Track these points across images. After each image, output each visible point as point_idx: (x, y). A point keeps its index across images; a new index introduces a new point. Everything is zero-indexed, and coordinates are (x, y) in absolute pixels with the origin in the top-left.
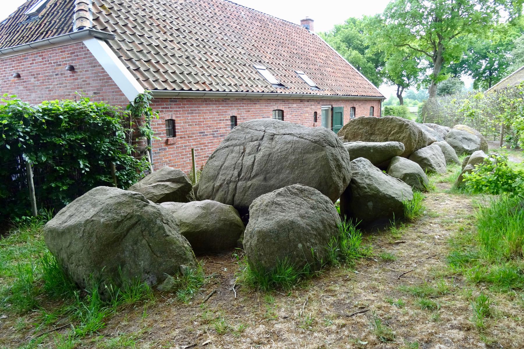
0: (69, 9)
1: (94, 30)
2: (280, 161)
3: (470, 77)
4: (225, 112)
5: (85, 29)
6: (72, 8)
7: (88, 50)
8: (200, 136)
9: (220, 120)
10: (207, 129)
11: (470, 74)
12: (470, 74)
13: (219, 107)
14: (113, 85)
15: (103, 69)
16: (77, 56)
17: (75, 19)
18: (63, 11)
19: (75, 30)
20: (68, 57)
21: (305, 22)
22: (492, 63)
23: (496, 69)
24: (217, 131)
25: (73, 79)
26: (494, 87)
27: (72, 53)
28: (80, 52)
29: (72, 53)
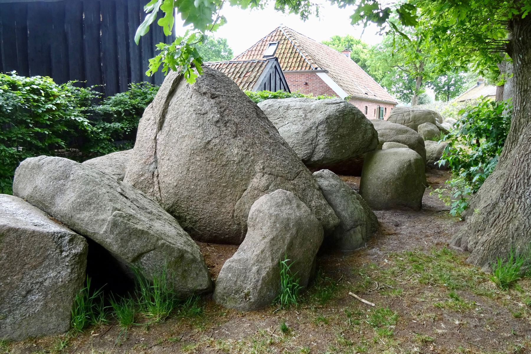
2: (419, 117)
3: (433, 90)
11: (433, 88)
12: (433, 88)
22: (450, 80)
23: (452, 85)
26: (452, 100)
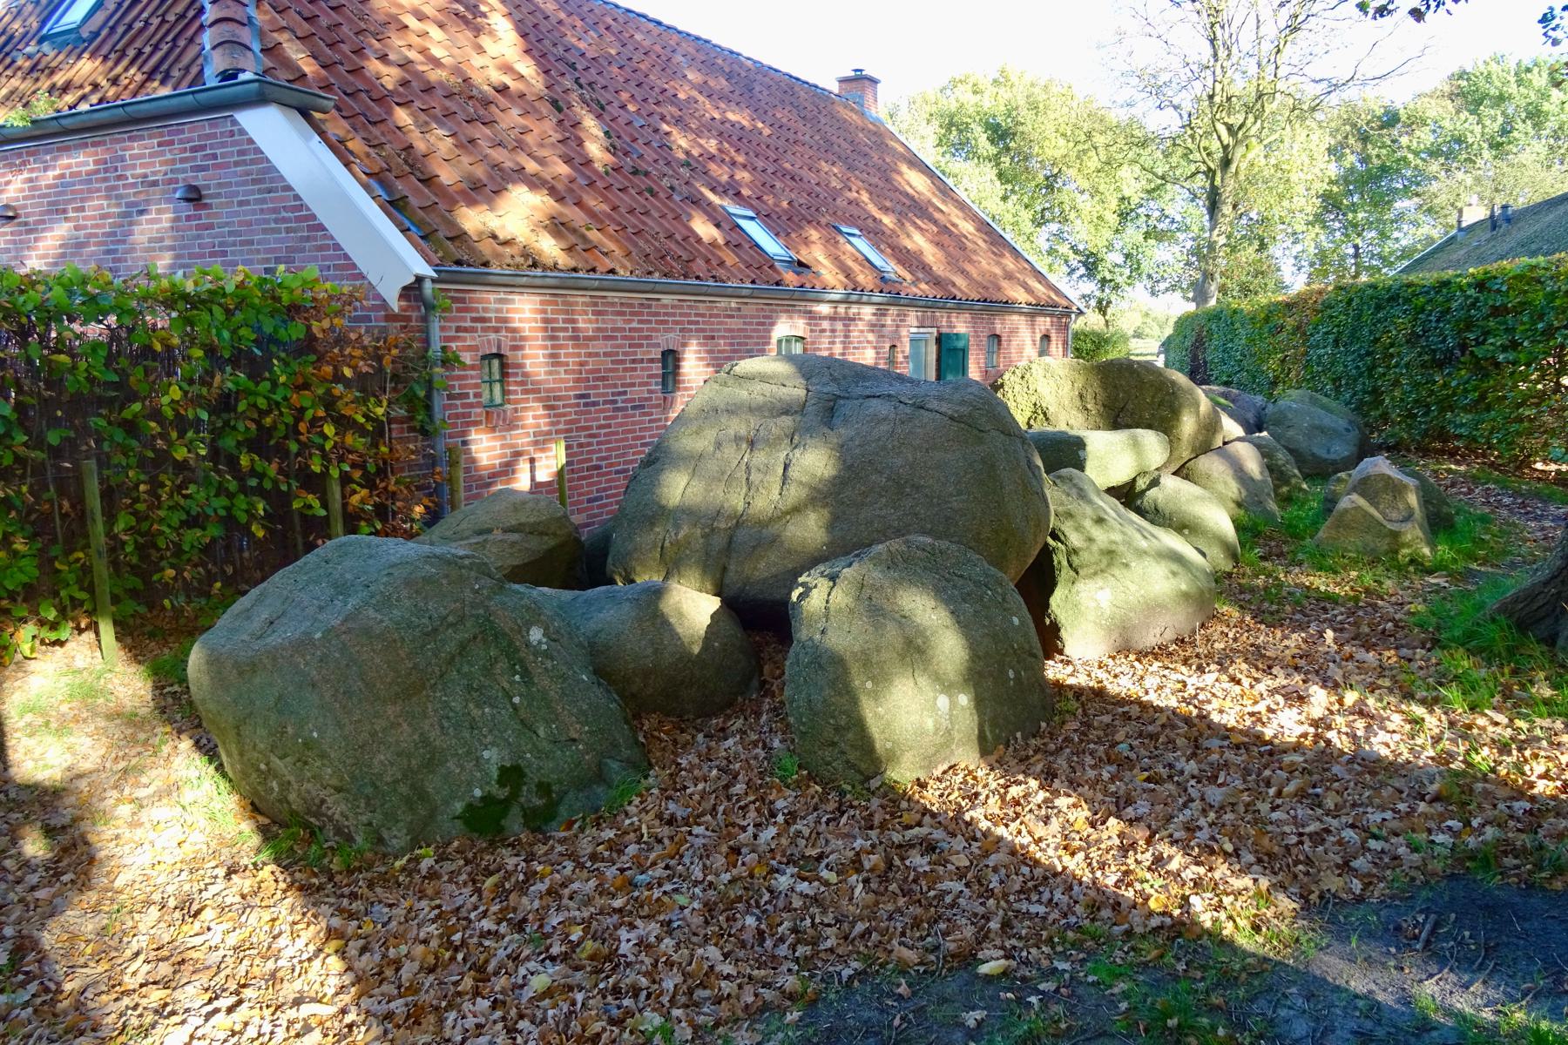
0: (182, 16)
1: (269, 79)
4: (647, 338)
5: (242, 77)
6: (191, 13)
7: (251, 141)
8: (578, 405)
9: (634, 361)
10: (596, 387)
13: (630, 321)
14: (327, 247)
15: (297, 197)
16: (215, 156)
17: (208, 47)
18: (164, 21)
19: (212, 82)
20: (182, 160)
21: (854, 85)
24: (625, 393)
25: (198, 227)
27: (194, 149)
28: (223, 144)
29: (194, 149)
